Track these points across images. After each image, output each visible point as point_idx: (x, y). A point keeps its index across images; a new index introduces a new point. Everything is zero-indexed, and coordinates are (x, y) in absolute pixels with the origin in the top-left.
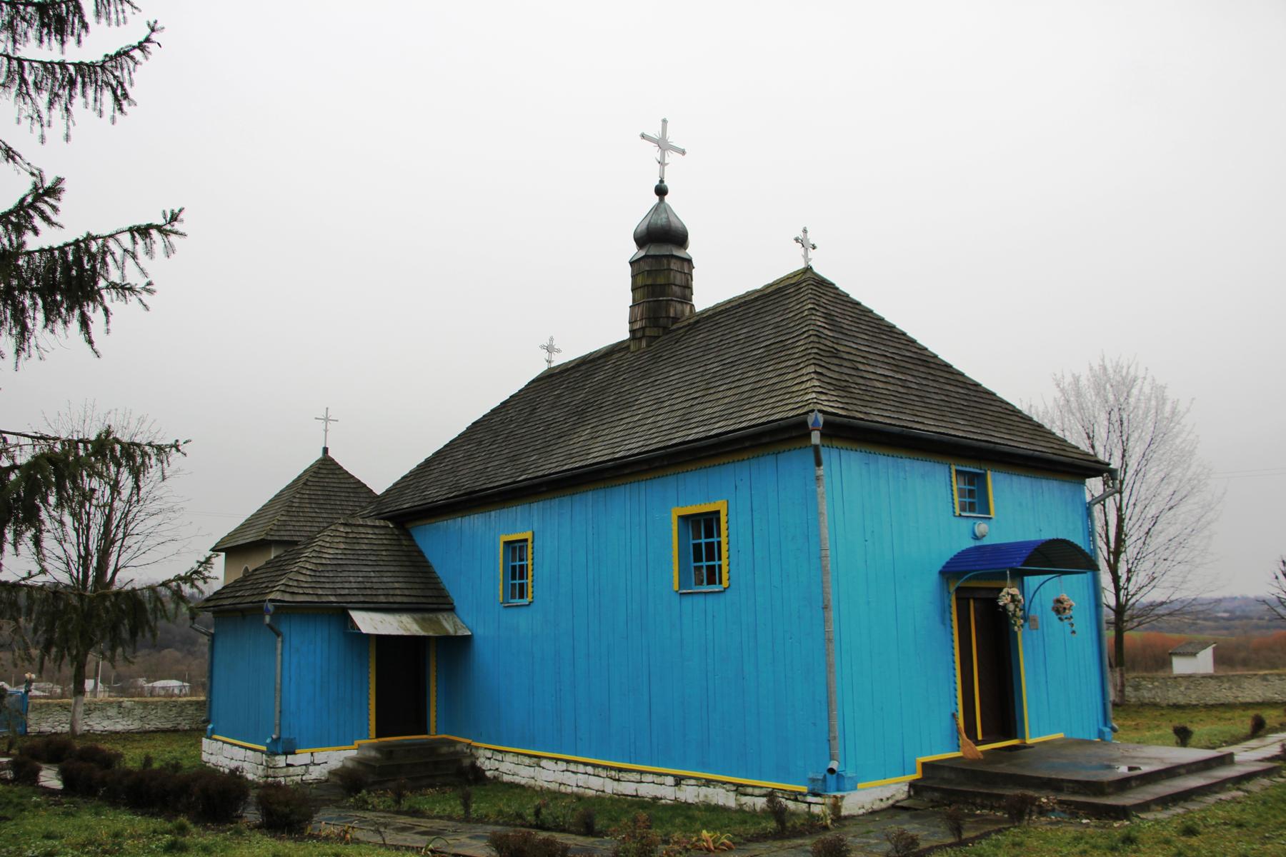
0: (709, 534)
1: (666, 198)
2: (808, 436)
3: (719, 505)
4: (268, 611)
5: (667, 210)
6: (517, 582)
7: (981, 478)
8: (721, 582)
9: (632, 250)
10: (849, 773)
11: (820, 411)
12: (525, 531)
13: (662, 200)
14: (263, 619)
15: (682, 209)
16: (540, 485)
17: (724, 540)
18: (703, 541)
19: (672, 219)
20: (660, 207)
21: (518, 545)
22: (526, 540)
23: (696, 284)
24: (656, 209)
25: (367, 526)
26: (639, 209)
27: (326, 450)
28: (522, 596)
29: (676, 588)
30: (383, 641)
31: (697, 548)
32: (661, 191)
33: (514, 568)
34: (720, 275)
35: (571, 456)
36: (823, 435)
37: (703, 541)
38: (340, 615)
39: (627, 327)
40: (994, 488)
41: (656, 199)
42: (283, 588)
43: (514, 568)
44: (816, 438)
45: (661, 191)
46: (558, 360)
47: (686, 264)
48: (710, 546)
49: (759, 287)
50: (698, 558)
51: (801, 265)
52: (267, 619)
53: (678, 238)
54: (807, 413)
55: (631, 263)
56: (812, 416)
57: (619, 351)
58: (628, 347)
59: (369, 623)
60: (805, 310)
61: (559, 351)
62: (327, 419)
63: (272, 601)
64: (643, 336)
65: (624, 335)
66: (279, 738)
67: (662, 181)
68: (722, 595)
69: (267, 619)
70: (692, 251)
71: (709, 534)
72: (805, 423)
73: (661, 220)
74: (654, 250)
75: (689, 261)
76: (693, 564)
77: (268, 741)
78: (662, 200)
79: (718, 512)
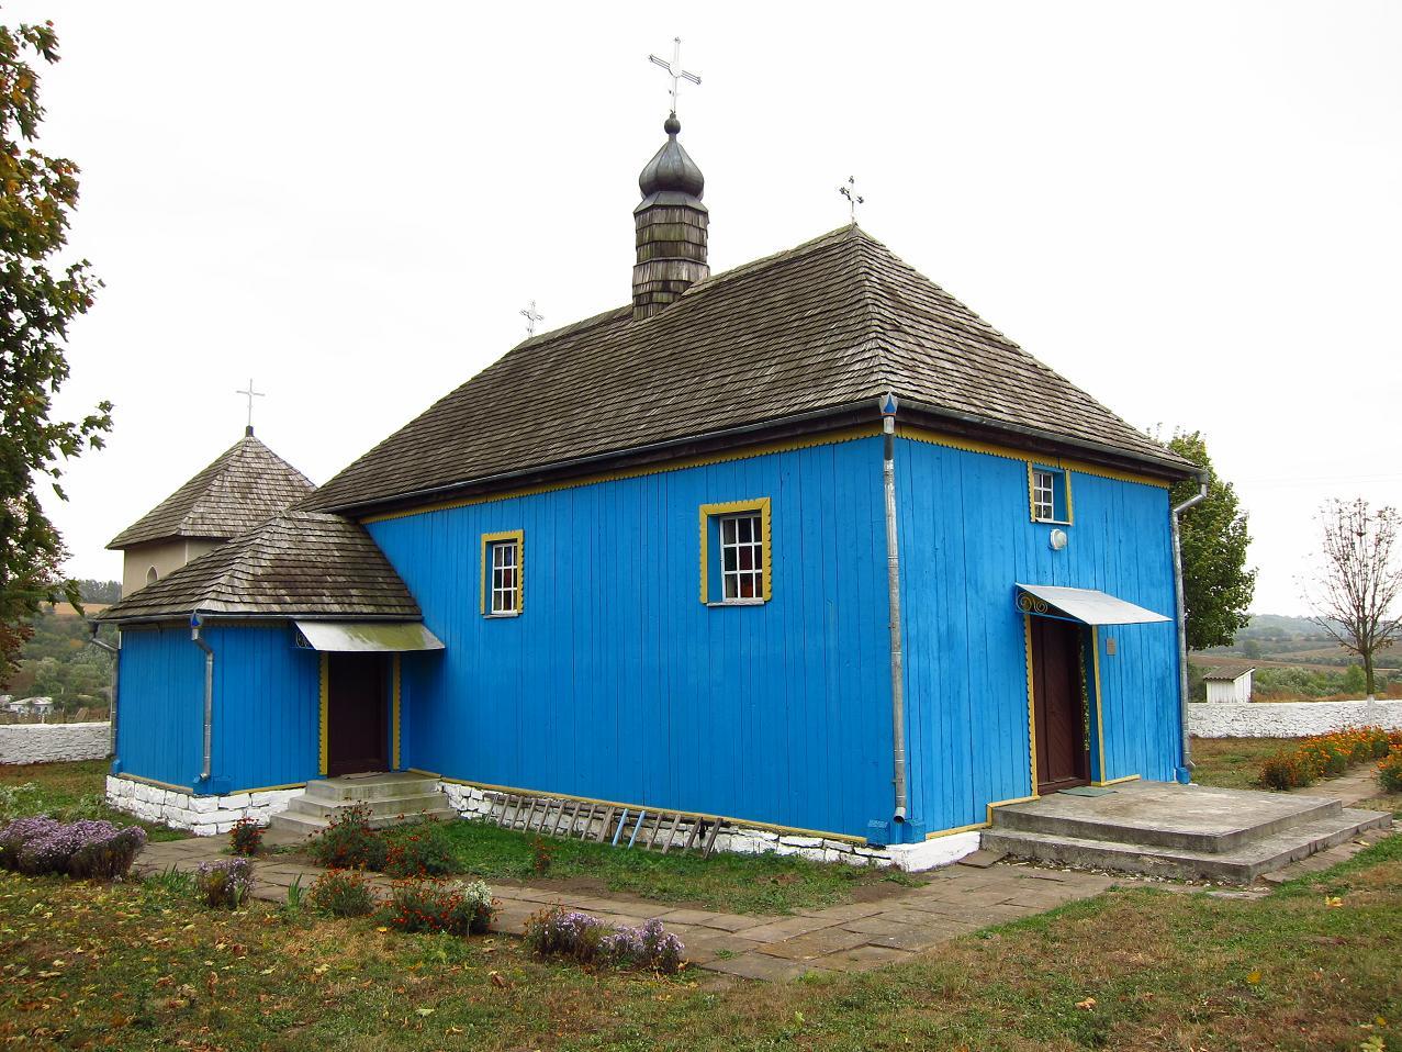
0: (745, 537)
1: (679, 137)
2: (881, 423)
3: (762, 503)
4: (196, 623)
5: (679, 150)
6: (502, 589)
7: (1059, 478)
8: (759, 594)
9: (636, 199)
10: (914, 823)
11: (894, 394)
12: (513, 529)
13: (672, 139)
14: (191, 635)
15: (699, 151)
16: (534, 475)
17: (765, 544)
18: (738, 545)
19: (686, 162)
20: (671, 148)
21: (503, 546)
22: (515, 541)
23: (712, 243)
24: (665, 149)
25: (313, 521)
26: (645, 149)
27: (250, 431)
28: (508, 607)
29: (704, 599)
30: (335, 657)
31: (730, 553)
32: (672, 128)
33: (498, 573)
34: (733, 244)
35: (791, 384)
36: (897, 425)
37: (738, 545)
38: (286, 630)
39: (630, 292)
40: (1074, 489)
41: (666, 137)
42: (214, 596)
43: (498, 573)
44: (889, 428)
45: (672, 128)
46: (541, 329)
47: (701, 218)
48: (745, 552)
49: (793, 246)
50: (731, 565)
51: (840, 222)
52: (196, 636)
53: (693, 186)
54: (879, 395)
55: (636, 214)
56: (885, 399)
57: (619, 319)
58: (630, 315)
59: (324, 638)
60: (832, 281)
61: (541, 318)
62: (250, 393)
63: (200, 611)
64: (651, 302)
65: (625, 299)
66: (209, 777)
67: (673, 115)
68: (762, 610)
69: (196, 636)
70: (708, 200)
71: (745, 537)
72: (876, 408)
73: (671, 165)
74: (664, 199)
75: (705, 214)
76: (724, 573)
77: (196, 780)
78: (672, 139)
79: (759, 511)
